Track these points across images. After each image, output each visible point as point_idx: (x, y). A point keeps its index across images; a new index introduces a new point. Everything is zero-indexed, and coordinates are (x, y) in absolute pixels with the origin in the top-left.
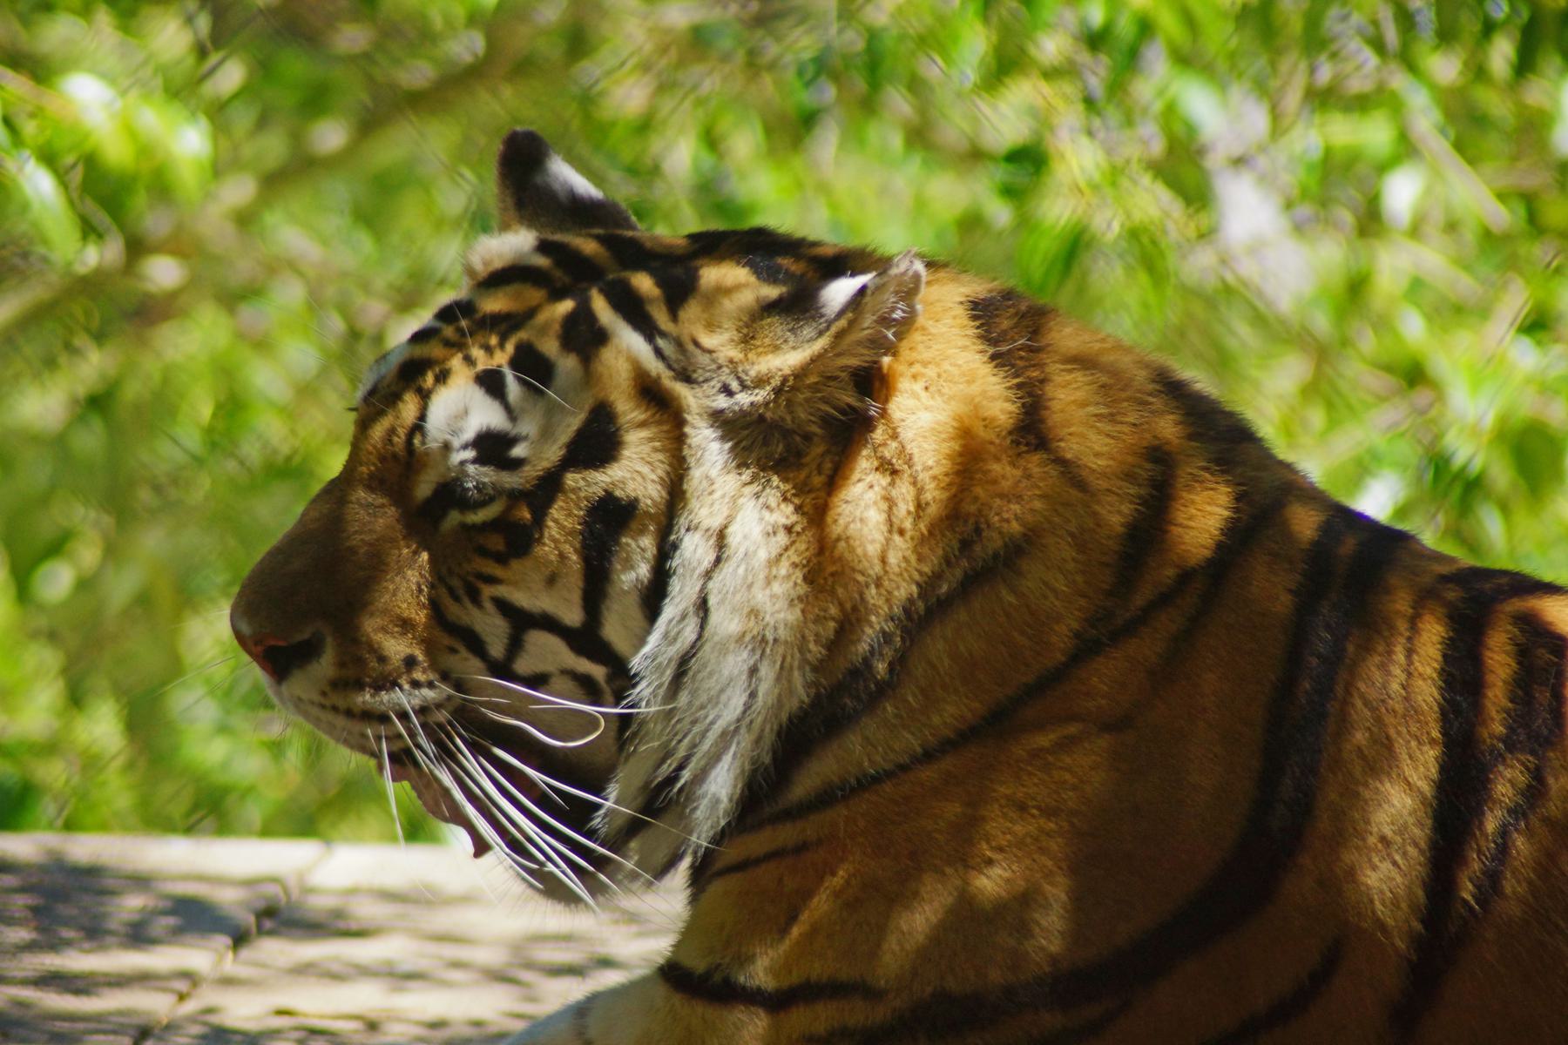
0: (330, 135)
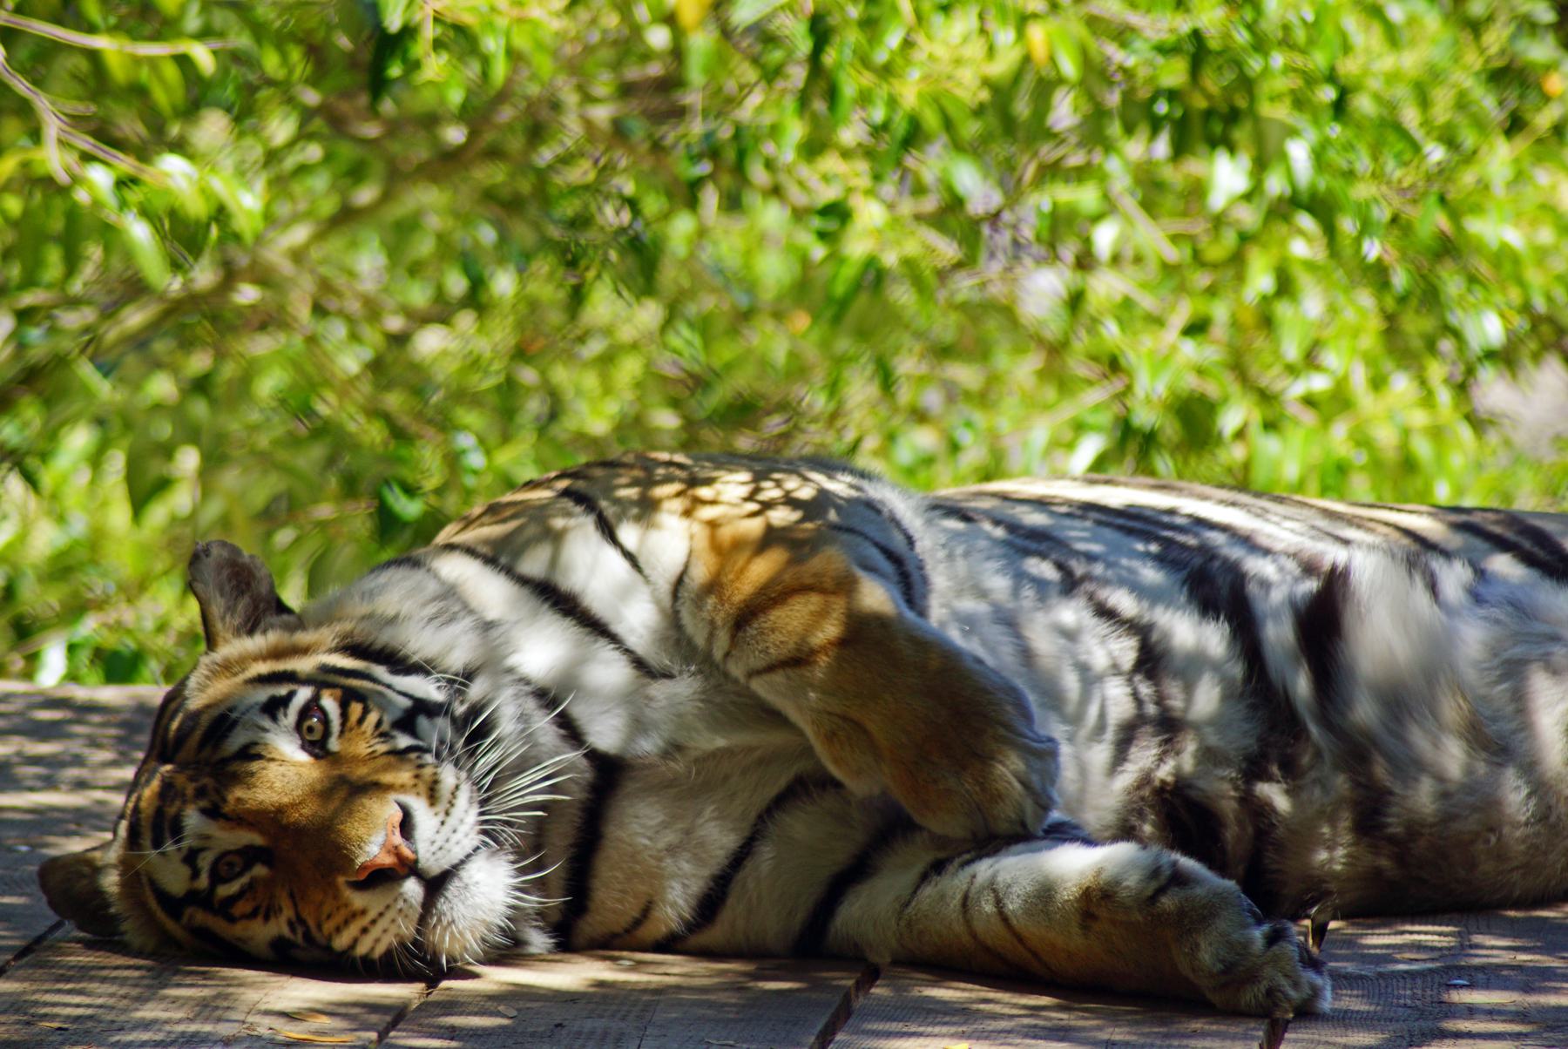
0: (366, 195)
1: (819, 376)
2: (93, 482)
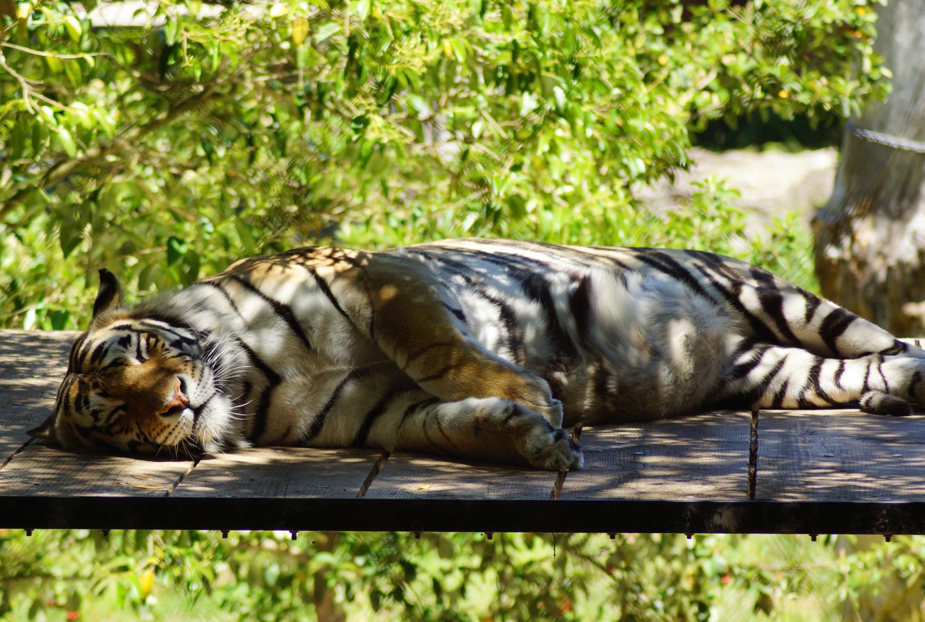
1: (357, 191)
2: (47, 239)
